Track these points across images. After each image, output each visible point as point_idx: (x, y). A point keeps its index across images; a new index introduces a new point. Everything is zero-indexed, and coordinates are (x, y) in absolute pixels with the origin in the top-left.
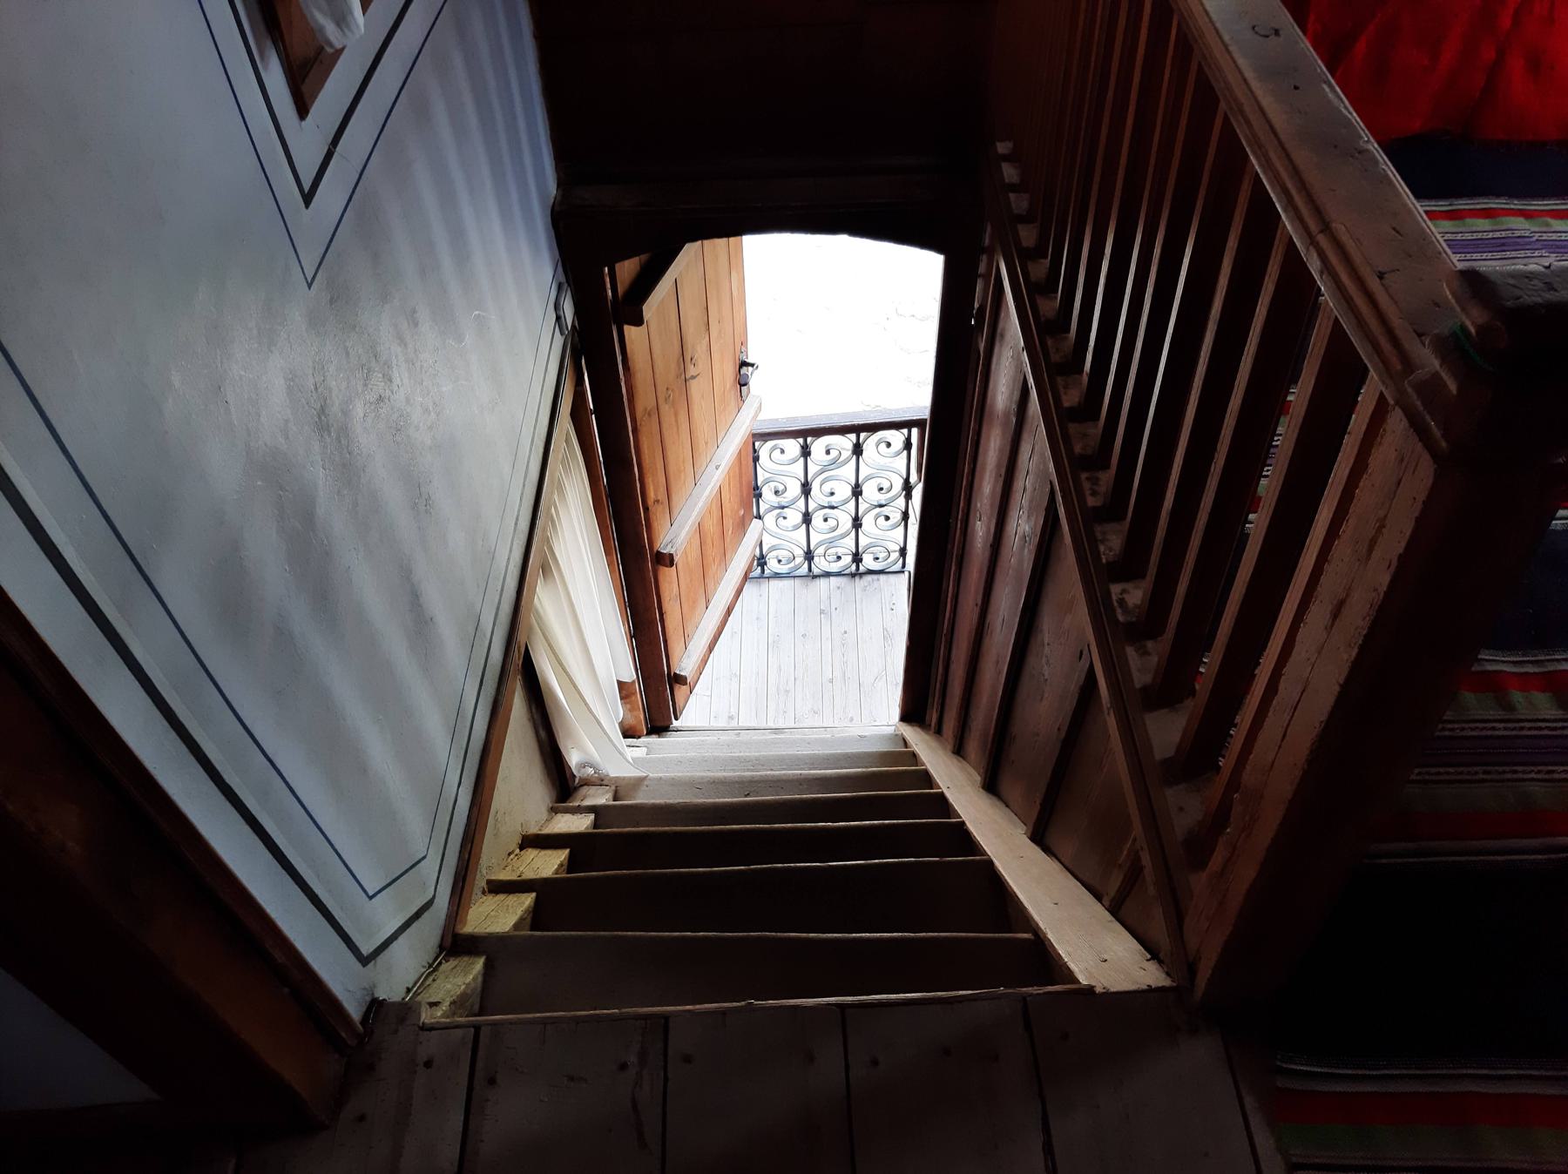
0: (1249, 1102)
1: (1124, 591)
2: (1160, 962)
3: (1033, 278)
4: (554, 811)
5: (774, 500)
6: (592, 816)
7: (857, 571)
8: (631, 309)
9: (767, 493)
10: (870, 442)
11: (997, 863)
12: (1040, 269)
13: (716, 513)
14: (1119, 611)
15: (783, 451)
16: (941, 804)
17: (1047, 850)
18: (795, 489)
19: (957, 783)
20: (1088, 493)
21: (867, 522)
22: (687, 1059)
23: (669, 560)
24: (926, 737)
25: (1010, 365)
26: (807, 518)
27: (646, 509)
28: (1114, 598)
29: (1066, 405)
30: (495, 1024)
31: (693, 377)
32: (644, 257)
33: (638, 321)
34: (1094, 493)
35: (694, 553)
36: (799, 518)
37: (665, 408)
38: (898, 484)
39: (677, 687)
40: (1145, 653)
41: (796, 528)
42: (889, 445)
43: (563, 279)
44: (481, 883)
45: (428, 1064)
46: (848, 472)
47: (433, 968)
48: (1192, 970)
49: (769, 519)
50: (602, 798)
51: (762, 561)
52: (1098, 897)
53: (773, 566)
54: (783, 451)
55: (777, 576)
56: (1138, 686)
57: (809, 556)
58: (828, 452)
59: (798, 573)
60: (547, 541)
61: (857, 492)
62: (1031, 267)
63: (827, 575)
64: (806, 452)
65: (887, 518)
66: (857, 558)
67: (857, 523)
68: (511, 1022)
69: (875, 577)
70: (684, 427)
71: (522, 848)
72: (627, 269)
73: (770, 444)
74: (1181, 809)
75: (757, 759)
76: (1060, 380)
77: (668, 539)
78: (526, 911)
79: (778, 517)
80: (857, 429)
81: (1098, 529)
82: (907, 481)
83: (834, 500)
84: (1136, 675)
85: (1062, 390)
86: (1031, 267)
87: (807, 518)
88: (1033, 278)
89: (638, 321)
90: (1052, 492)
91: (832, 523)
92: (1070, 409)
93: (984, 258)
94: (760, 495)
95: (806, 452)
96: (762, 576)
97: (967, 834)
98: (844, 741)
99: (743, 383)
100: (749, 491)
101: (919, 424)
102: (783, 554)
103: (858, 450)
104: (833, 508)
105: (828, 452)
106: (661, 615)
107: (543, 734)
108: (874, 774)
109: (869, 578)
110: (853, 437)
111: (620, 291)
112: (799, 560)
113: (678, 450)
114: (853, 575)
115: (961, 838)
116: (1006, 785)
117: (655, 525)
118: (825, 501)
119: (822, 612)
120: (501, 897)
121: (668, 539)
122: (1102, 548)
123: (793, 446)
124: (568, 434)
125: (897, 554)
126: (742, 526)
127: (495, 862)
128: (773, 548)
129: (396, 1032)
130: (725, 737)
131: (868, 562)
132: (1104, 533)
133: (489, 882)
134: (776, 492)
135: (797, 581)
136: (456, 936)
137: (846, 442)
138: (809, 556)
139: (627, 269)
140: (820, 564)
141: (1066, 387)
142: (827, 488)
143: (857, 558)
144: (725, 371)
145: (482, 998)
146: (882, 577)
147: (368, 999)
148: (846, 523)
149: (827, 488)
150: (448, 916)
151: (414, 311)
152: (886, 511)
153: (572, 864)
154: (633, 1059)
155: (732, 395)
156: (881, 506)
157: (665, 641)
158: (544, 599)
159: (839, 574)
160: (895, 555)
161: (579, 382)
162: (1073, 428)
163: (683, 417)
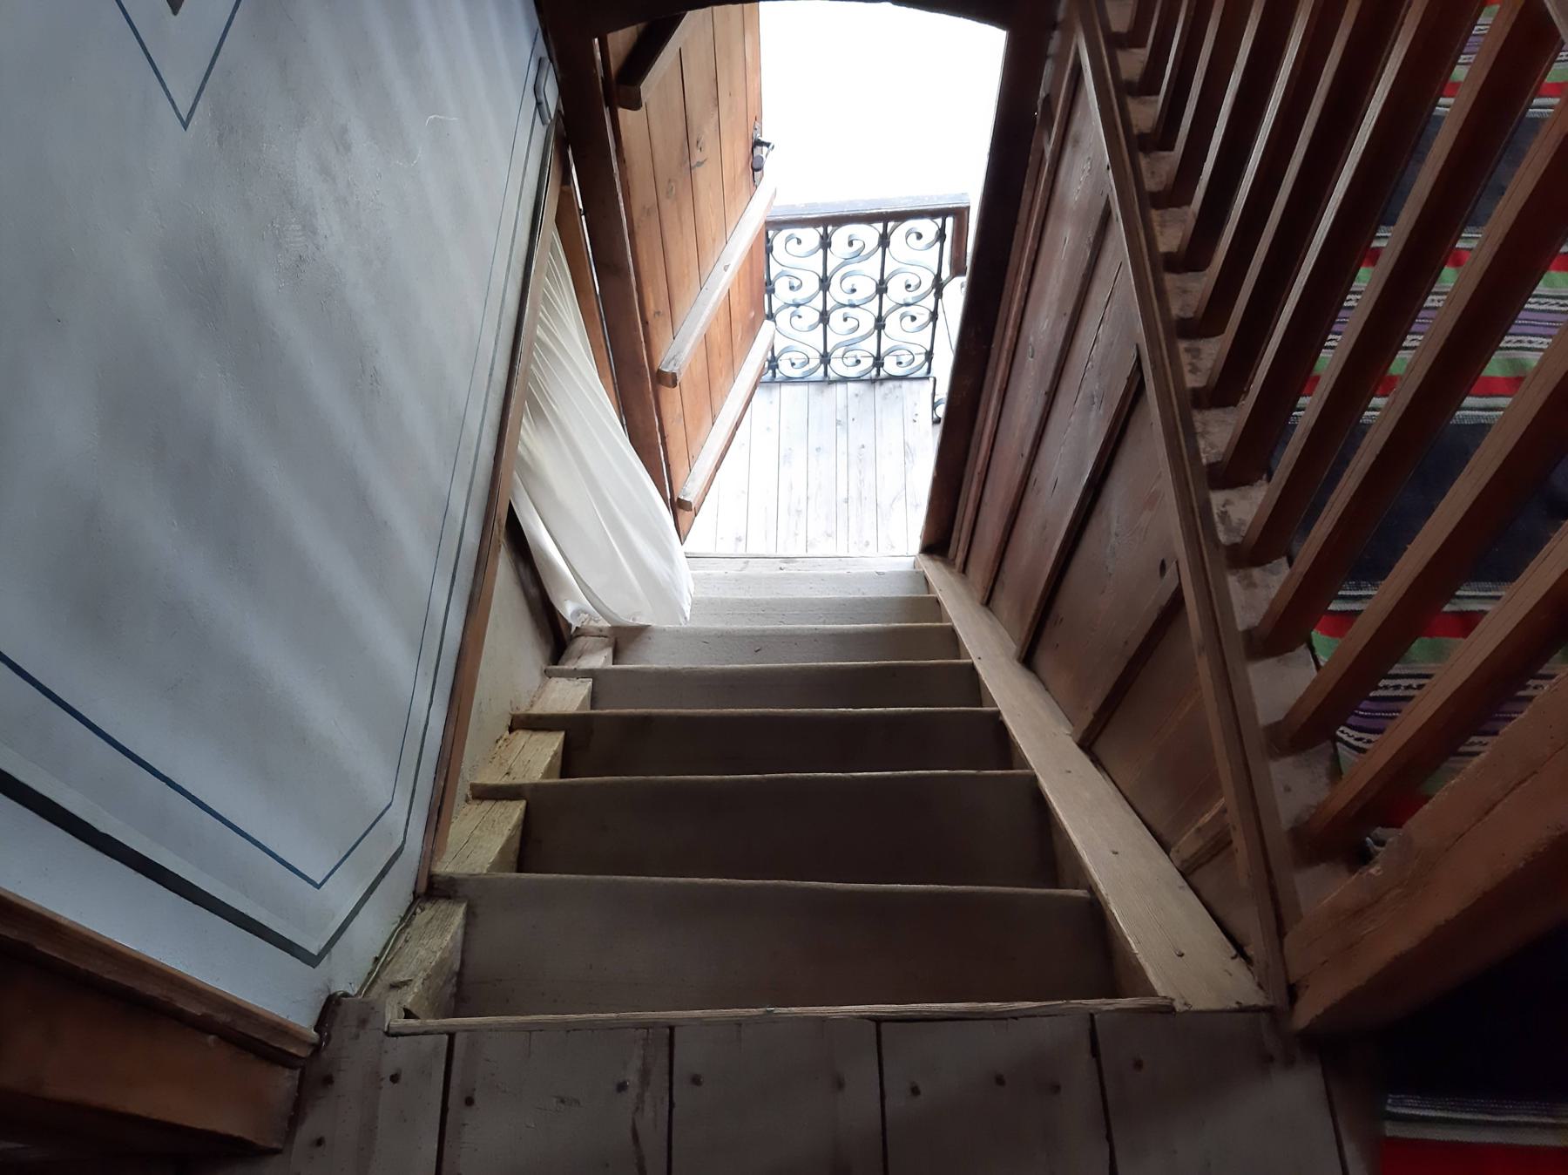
0: (1350, 1150)
1: (1227, 503)
2: (1248, 960)
3: (1124, 76)
4: (548, 674)
5: (790, 297)
6: (589, 682)
7: (877, 376)
8: (626, 83)
9: (781, 286)
10: (899, 233)
11: (1041, 780)
12: (1133, 62)
13: (723, 320)
14: (1220, 528)
15: (799, 242)
16: (969, 682)
17: (1097, 762)
18: (812, 284)
19: (987, 647)
20: (1186, 369)
21: (891, 322)
22: (696, 1080)
23: (673, 380)
24: (952, 578)
25: (1085, 168)
26: (824, 317)
27: (645, 323)
28: (1215, 511)
29: (1162, 248)
30: (469, 1030)
31: (700, 164)
32: (641, 26)
33: (635, 103)
34: (1194, 370)
35: (700, 367)
36: (816, 316)
37: (666, 204)
38: (928, 282)
39: (681, 512)
40: (1251, 585)
41: (813, 327)
42: (919, 236)
43: (544, 54)
44: (463, 789)
45: (395, 1078)
46: (872, 267)
47: (407, 919)
48: (1293, 993)
49: (783, 318)
50: (599, 660)
51: (773, 363)
52: (1166, 847)
53: (785, 368)
54: (799, 242)
55: (789, 380)
56: (1241, 627)
57: (825, 358)
58: (851, 244)
59: (812, 377)
60: (527, 371)
61: (882, 288)
62: (1121, 56)
63: (845, 380)
64: (825, 243)
65: (914, 318)
66: (878, 362)
67: (880, 324)
68: (491, 1029)
69: (897, 383)
70: (688, 206)
71: (511, 730)
72: (621, 40)
73: (786, 233)
74: (1288, 789)
75: (768, 602)
76: (1155, 215)
77: (670, 354)
78: (516, 827)
79: (793, 315)
80: (884, 218)
81: (1198, 417)
82: (938, 277)
83: (855, 298)
84: (1238, 621)
85: (1157, 228)
86: (1121, 56)
87: (824, 317)
88: (1124, 76)
89: (635, 103)
90: (1139, 360)
91: (851, 323)
92: (1168, 255)
93: (1056, 34)
94: (773, 291)
95: (825, 243)
96: (773, 381)
97: (1002, 725)
98: (861, 578)
99: (756, 168)
100: (760, 283)
101: (960, 214)
102: (798, 358)
103: (884, 241)
104: (853, 306)
105: (851, 244)
106: (663, 438)
107: (533, 591)
108: (895, 630)
109: (890, 384)
110: (879, 226)
111: (614, 66)
112: (815, 362)
113: (682, 249)
114: (873, 381)
115: (996, 740)
116: (1044, 659)
117: (656, 340)
118: (844, 299)
119: (838, 423)
120: (487, 805)
121: (670, 354)
122: (1202, 444)
123: (812, 236)
124: (553, 245)
125: (923, 357)
126: (752, 330)
127: (479, 769)
128: (786, 350)
129: (357, 1036)
130: (733, 568)
131: (890, 366)
132: (1205, 424)
133: (473, 787)
134: (792, 288)
135: (812, 387)
136: (431, 877)
137: (869, 234)
138: (825, 358)
139: (621, 40)
140: (838, 367)
141: (1163, 225)
142: (847, 284)
143: (878, 362)
144: (736, 153)
145: (463, 952)
146: (905, 384)
147: (323, 998)
148: (868, 323)
149: (847, 284)
150: (423, 857)
151: (344, 130)
152: (912, 310)
153: (568, 762)
154: (632, 1078)
155: (744, 181)
156: (907, 305)
157: (668, 466)
158: (531, 440)
159: (857, 380)
160: (920, 359)
161: (565, 179)
162: (1170, 280)
163: (688, 206)
